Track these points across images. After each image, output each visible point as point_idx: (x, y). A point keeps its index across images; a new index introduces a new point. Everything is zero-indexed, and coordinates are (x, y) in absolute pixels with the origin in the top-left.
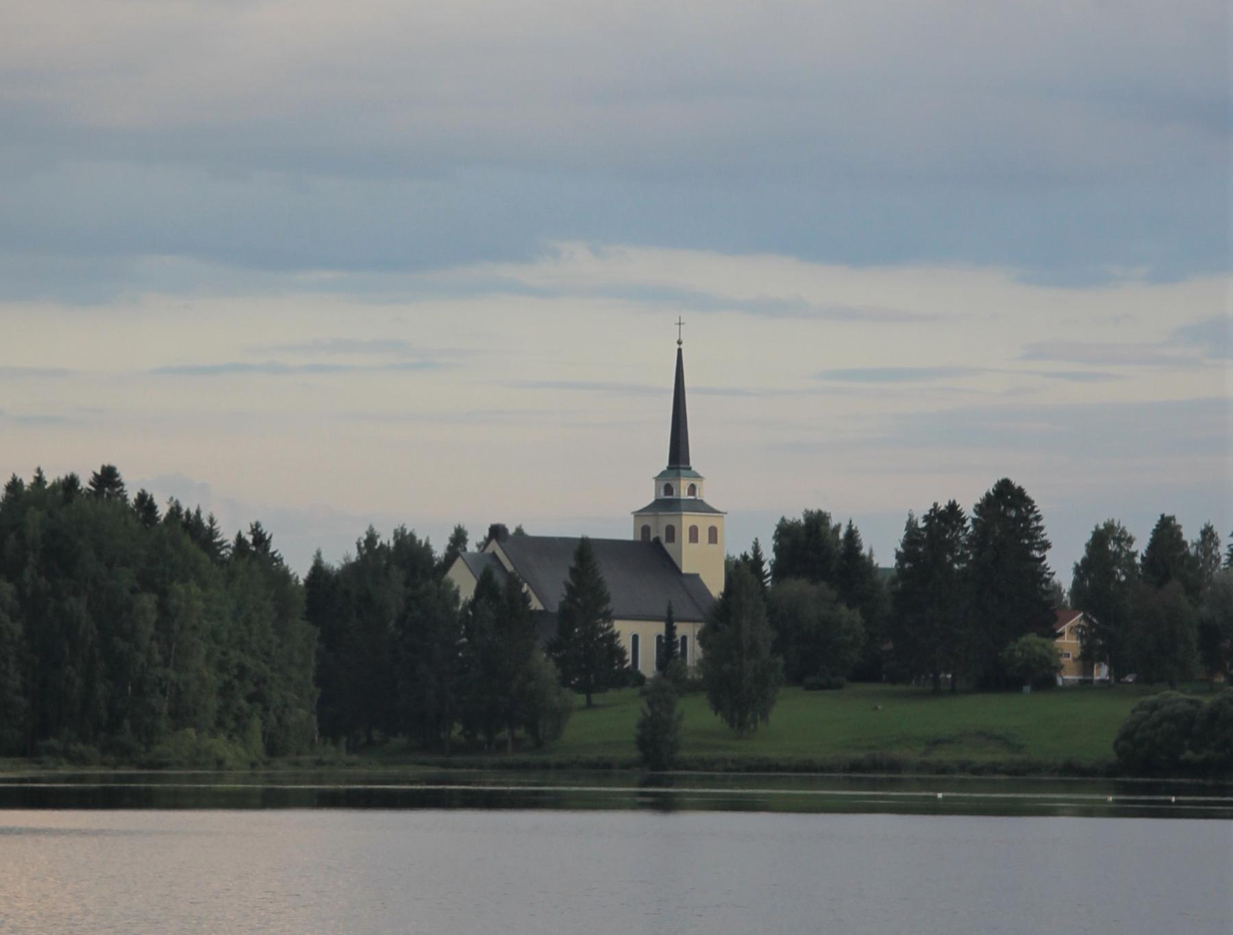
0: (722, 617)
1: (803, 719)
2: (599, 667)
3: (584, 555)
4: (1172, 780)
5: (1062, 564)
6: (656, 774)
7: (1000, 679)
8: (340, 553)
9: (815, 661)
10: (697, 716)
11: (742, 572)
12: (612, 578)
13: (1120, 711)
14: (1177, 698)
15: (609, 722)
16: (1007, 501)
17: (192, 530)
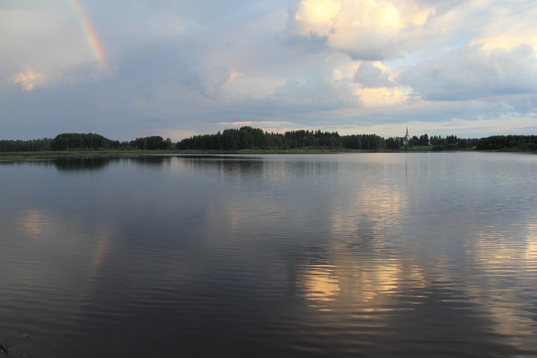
0: (410, 142)
1: (414, 147)
2: (403, 144)
3: (402, 138)
4: (412, 309)
5: (429, 138)
6: (406, 150)
7: (426, 145)
8: (388, 138)
9: (415, 144)
10: (408, 147)
11: (411, 139)
12: (403, 140)
13: (432, 147)
14: (436, 146)
15: (403, 148)
16: (426, 135)
17: (379, 137)
